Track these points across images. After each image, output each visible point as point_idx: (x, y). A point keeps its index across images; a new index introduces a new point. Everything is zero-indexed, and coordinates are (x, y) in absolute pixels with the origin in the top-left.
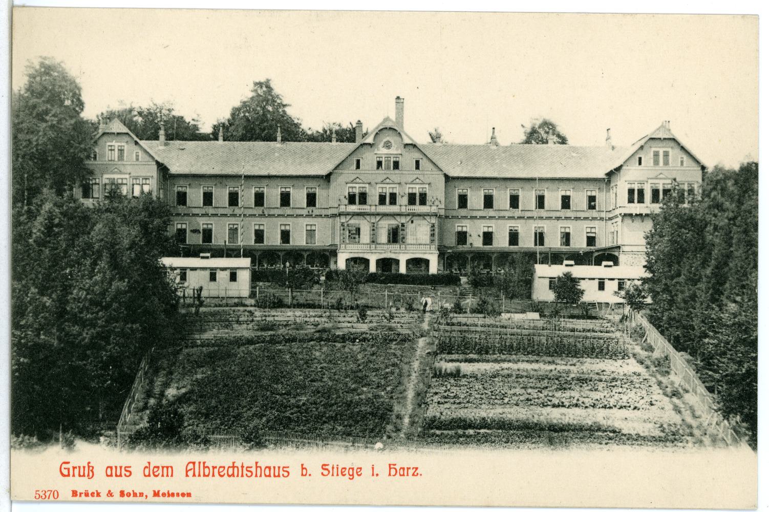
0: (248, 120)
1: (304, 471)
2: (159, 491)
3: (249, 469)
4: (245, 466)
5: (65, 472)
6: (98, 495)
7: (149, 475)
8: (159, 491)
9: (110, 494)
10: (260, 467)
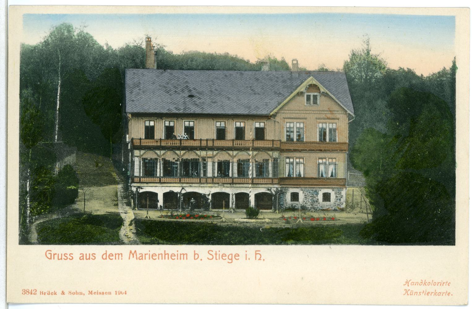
0: (165, 70)
1: (196, 256)
2: (92, 291)
3: (94, 255)
4: (434, 281)
5: (49, 256)
6: (55, 294)
7: (106, 259)
8: (92, 291)
9: (63, 293)
10: (168, 254)
